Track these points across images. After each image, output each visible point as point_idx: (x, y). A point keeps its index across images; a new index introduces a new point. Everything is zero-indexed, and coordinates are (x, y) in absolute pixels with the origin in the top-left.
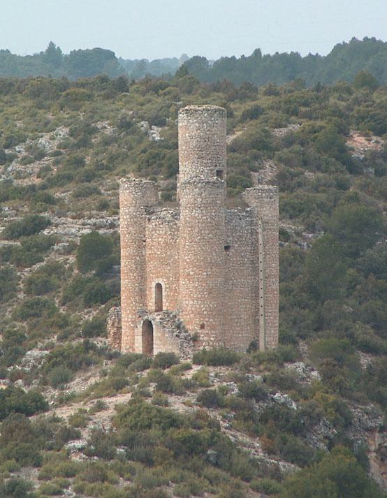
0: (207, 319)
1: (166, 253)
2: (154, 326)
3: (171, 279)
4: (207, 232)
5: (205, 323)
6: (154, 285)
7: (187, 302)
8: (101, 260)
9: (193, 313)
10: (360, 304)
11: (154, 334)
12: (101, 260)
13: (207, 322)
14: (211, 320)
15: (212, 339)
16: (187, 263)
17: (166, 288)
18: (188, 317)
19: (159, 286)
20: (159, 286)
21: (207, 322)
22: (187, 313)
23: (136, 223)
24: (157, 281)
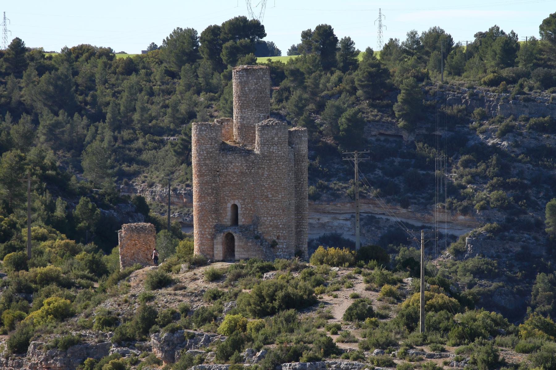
0: (281, 231)
1: (242, 181)
2: (236, 238)
3: (247, 200)
4: (281, 163)
5: (280, 234)
6: (229, 205)
7: (265, 218)
8: (473, 170)
9: (271, 226)
10: (377, 326)
11: (236, 244)
12: (473, 170)
13: (282, 233)
14: (284, 232)
15: (284, 246)
16: (266, 188)
17: (242, 208)
18: (267, 230)
19: (235, 207)
20: (235, 207)
21: (282, 233)
22: (265, 226)
23: (211, 157)
24: (232, 202)
